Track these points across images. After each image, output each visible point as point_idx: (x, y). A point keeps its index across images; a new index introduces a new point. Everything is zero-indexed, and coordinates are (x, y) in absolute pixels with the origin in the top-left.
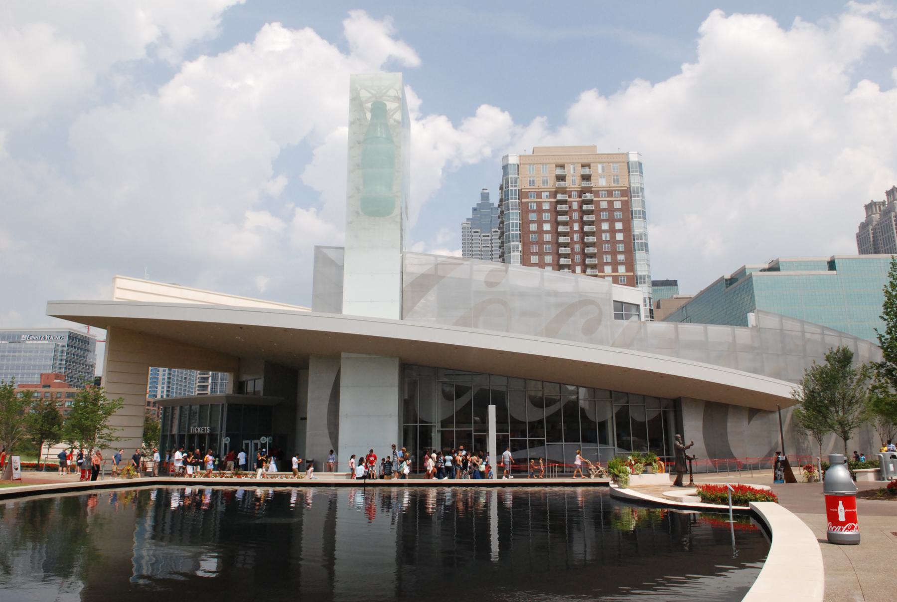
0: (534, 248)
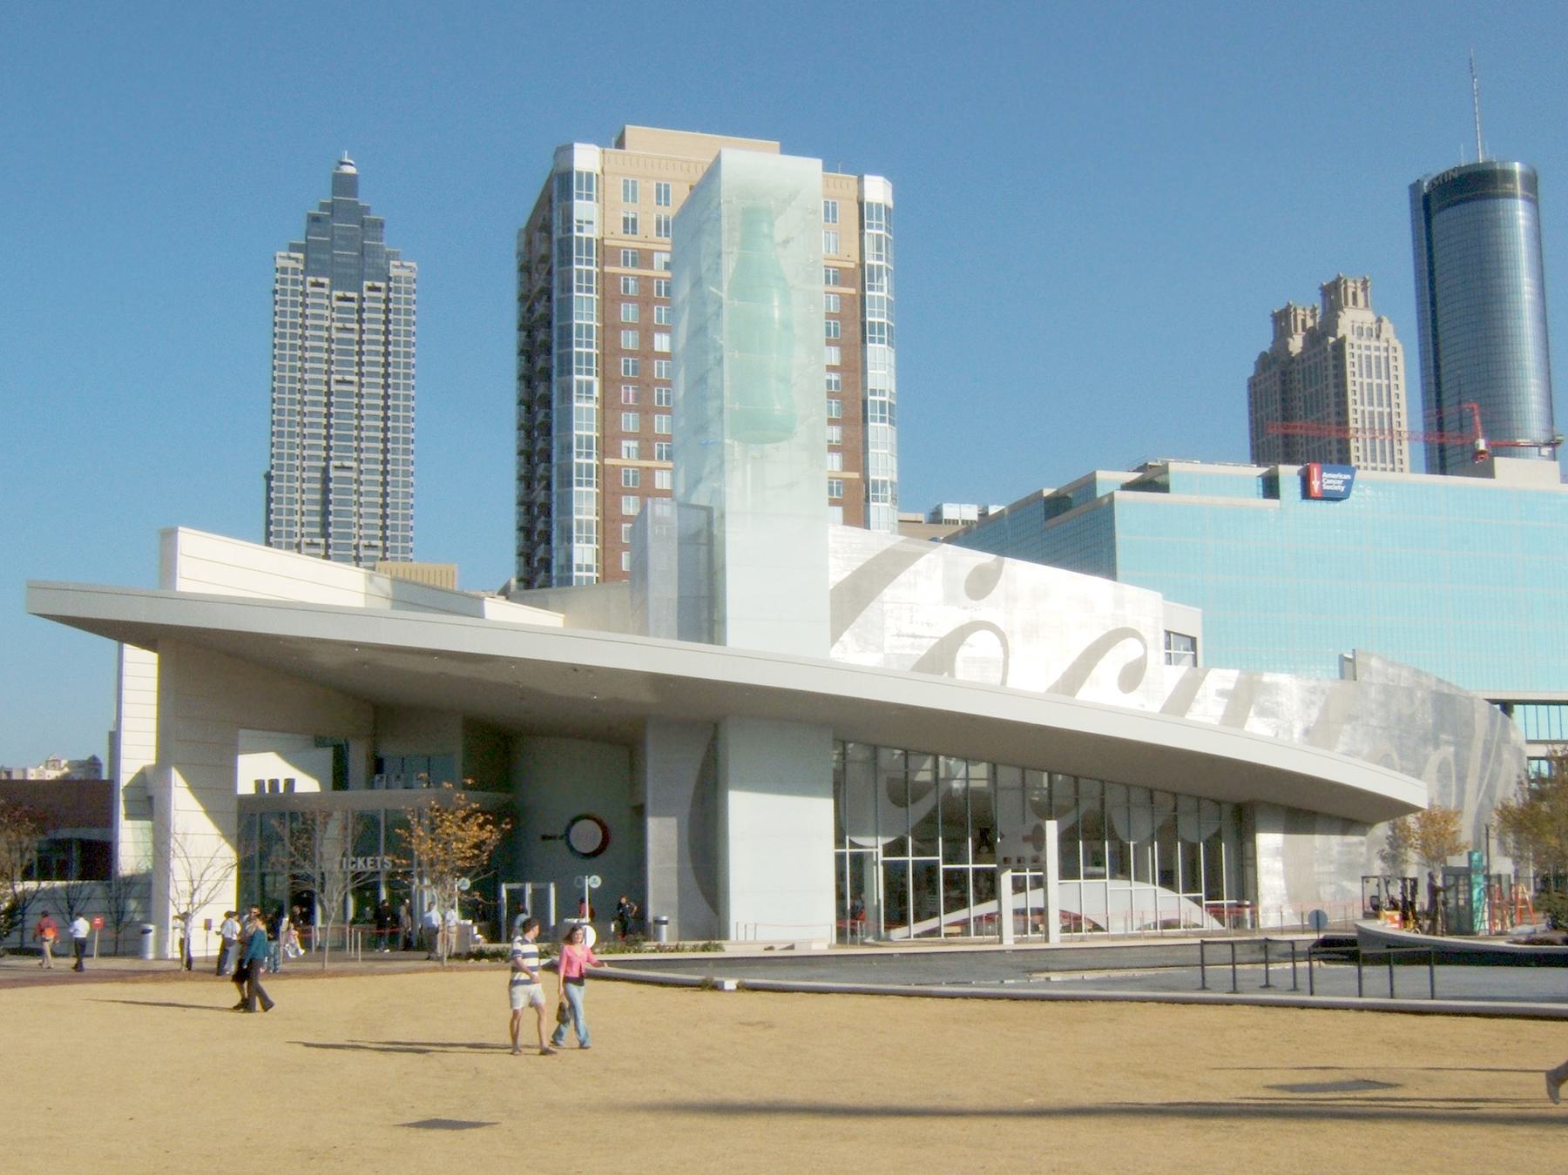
0: (628, 394)
